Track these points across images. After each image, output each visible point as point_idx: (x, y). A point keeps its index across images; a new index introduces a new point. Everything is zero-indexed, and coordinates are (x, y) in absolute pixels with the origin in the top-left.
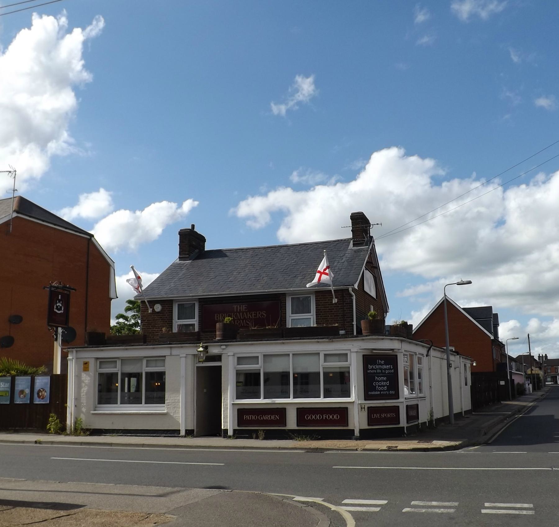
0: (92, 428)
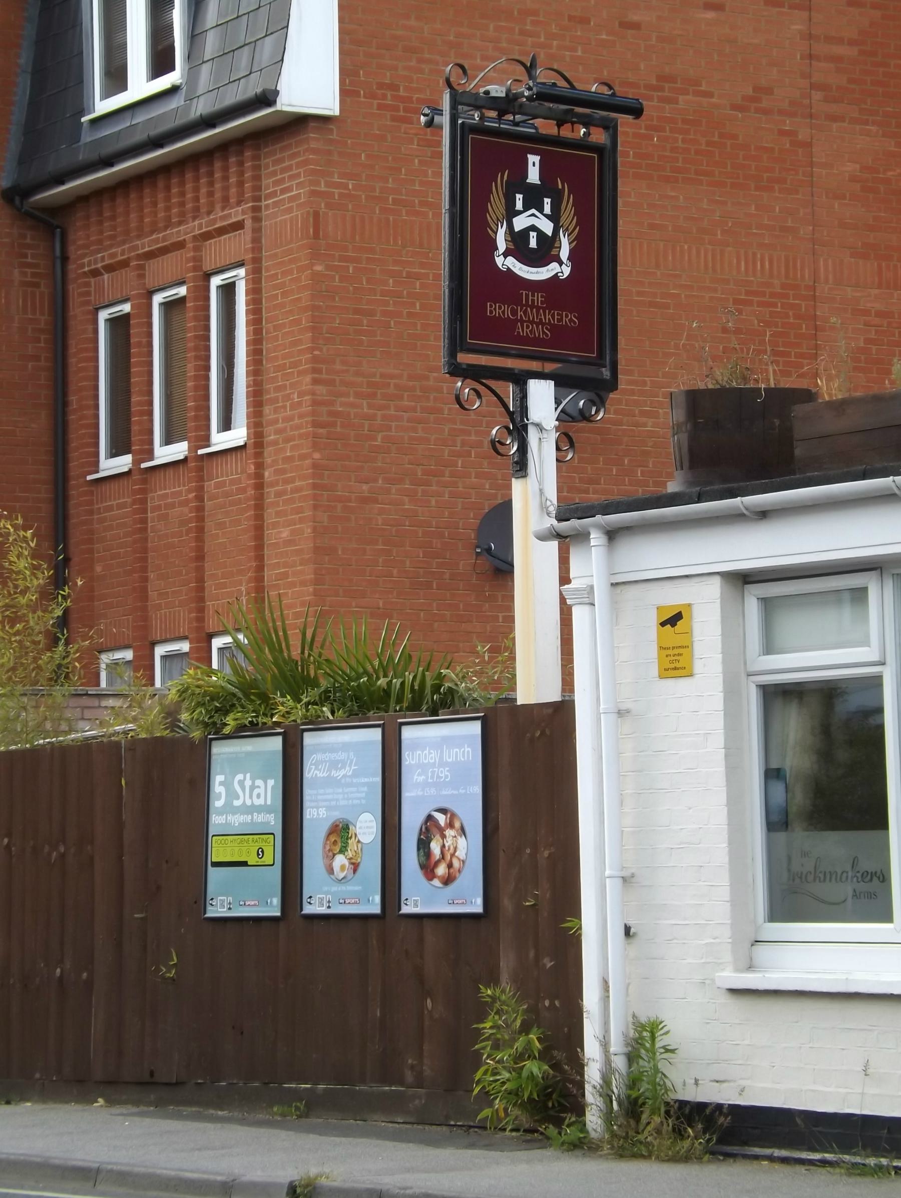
0: (728, 1096)
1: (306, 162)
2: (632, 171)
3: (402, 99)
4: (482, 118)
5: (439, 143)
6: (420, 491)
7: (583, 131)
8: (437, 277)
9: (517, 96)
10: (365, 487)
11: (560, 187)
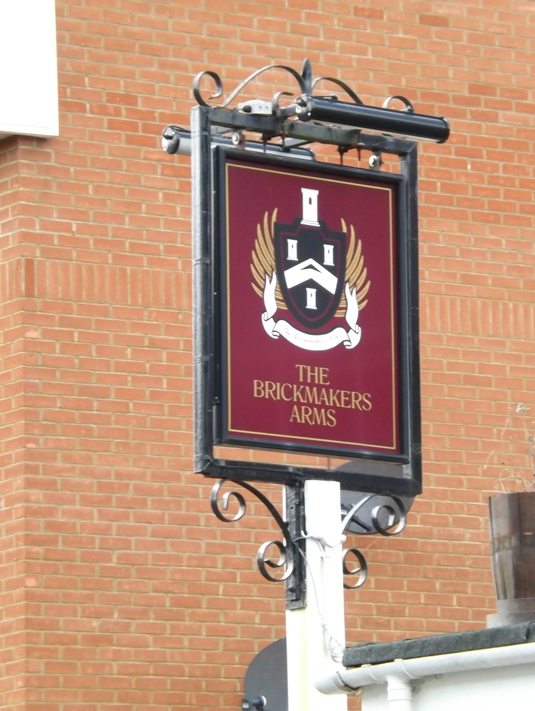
1: (15, 196)
2: (439, 207)
3: (142, 115)
4: (242, 142)
5: (188, 172)
6: (168, 627)
7: (372, 158)
8: (188, 345)
9: (285, 115)
10: (96, 623)
11: (345, 230)
